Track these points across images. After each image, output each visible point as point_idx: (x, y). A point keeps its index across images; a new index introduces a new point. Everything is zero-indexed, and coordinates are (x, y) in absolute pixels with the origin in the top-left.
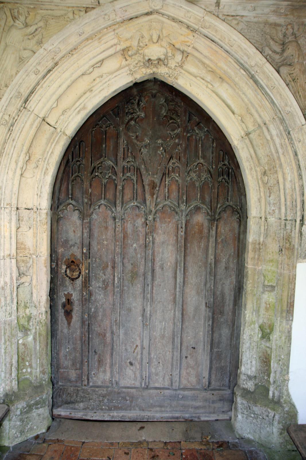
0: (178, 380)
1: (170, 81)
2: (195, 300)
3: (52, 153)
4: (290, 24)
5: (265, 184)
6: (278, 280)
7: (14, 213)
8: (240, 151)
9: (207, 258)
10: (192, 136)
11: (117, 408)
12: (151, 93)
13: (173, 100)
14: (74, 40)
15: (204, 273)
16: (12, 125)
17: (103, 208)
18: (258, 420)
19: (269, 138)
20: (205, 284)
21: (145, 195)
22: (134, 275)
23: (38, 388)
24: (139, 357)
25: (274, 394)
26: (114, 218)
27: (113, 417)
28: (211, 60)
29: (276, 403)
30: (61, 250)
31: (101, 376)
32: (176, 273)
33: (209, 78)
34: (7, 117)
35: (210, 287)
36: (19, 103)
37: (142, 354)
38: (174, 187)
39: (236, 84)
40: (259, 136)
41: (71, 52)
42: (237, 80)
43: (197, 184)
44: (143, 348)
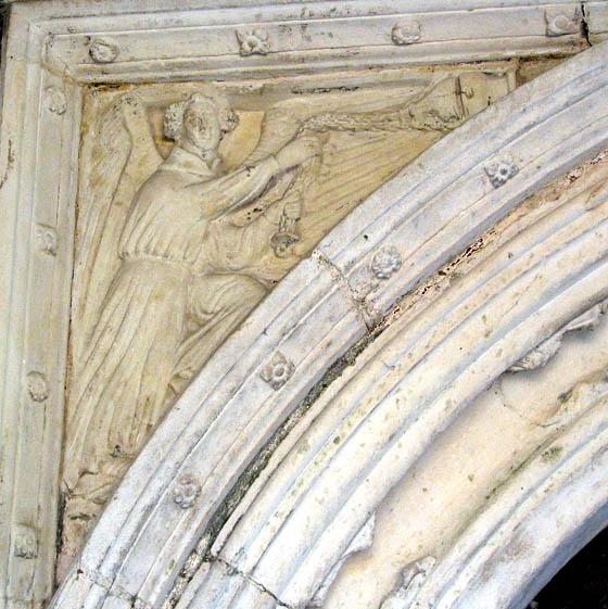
14: (466, 208)
36: (183, 532)
41: (447, 269)
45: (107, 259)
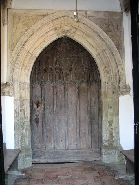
0: (79, 146)
1: (71, 37)
2: (84, 115)
3: (31, 63)
4: (109, 19)
5: (106, 71)
6: (113, 103)
7: (19, 84)
8: (97, 60)
9: (87, 98)
10: (79, 56)
11: (57, 158)
12: (64, 42)
13: (72, 44)
14: (39, 26)
15: (87, 105)
16: (19, 54)
17: (48, 83)
18: (110, 155)
19: (106, 55)
20: (87, 109)
21: (63, 77)
22: (61, 107)
23: (28, 150)
24: (64, 138)
25: (115, 145)
26: (53, 86)
27: (55, 161)
28: (85, 30)
29: (116, 148)
30: (34, 99)
31: (50, 146)
32: (76, 105)
33: (84, 36)
34: (17, 51)
35: (89, 110)
36: (21, 46)
37: (65, 136)
38: (74, 74)
39: (93, 38)
40: (103, 54)
41: (38, 30)
42: (94, 36)
43: (82, 73)
44: (65, 134)
45: (16, 27)
